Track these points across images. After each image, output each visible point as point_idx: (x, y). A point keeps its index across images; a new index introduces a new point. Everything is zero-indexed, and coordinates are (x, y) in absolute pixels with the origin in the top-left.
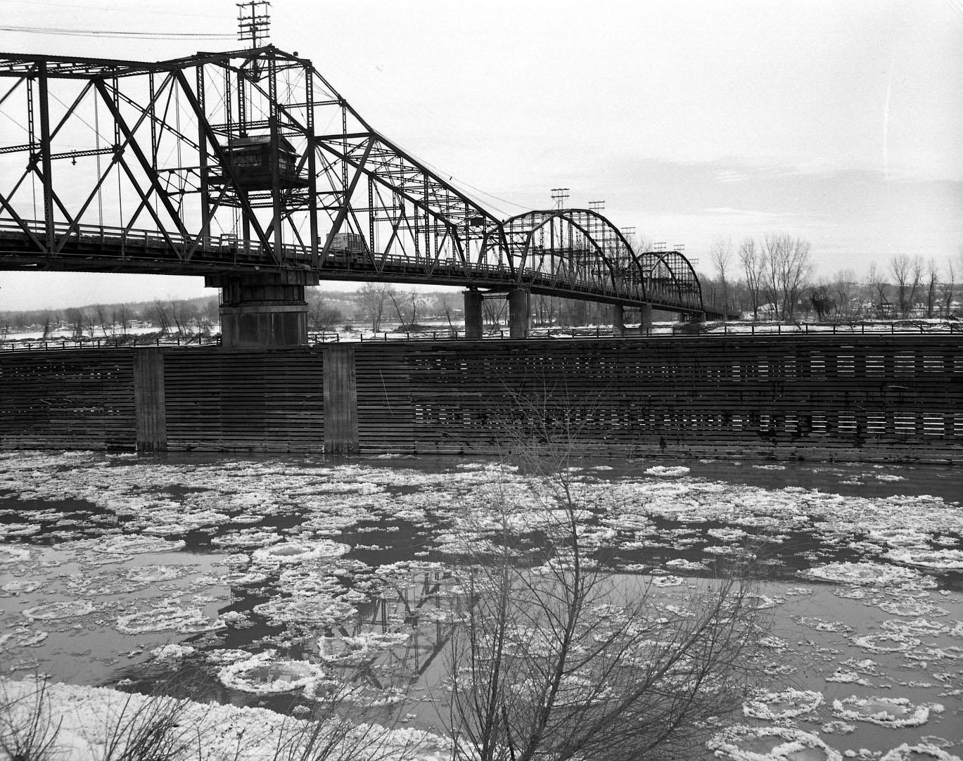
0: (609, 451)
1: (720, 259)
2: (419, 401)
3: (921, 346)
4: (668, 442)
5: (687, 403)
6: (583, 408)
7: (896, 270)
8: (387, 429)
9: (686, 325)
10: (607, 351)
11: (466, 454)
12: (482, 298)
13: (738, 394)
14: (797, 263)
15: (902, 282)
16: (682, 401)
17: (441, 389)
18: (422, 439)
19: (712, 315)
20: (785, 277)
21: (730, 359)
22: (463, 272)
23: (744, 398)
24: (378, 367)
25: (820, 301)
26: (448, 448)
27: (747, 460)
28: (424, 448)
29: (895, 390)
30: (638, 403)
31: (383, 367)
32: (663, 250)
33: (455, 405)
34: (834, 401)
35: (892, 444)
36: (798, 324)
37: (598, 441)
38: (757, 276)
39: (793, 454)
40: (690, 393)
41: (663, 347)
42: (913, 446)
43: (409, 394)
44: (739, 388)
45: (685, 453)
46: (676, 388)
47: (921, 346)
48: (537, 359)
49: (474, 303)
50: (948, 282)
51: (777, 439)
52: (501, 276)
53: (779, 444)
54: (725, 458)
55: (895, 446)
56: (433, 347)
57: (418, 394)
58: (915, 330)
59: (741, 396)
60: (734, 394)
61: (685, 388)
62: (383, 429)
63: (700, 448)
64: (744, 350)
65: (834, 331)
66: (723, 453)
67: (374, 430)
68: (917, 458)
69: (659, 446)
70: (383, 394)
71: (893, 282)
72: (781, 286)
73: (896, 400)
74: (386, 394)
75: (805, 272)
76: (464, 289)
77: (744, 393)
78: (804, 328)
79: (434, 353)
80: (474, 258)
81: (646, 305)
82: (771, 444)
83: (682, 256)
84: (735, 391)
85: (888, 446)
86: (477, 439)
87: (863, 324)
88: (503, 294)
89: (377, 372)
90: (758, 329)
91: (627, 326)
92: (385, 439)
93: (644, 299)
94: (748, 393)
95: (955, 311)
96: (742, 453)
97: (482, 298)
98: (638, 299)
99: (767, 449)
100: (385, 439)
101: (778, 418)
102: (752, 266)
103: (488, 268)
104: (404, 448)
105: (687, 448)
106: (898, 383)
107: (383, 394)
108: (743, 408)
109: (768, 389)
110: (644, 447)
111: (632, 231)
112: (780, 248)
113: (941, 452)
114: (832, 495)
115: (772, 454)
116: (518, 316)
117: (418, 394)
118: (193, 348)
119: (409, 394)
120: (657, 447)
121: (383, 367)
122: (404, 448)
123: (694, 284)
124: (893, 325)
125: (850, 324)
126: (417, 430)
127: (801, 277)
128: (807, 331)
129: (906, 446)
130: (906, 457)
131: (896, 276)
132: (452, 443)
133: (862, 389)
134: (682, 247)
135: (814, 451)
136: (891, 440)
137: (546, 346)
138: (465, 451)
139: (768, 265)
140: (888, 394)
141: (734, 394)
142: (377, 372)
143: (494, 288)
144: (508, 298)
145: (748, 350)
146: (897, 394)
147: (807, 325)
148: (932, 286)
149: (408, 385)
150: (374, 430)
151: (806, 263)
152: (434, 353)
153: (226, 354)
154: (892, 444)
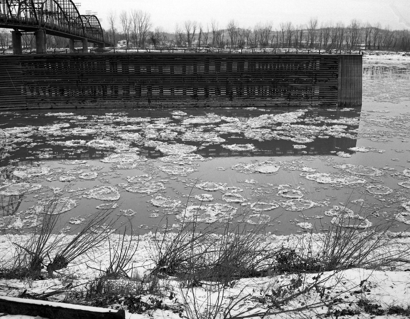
0: (125, 105)
1: (111, 19)
2: (27, 84)
3: (245, 58)
4: (152, 101)
5: (160, 83)
6: (112, 86)
7: (186, 27)
8: (11, 98)
9: (97, 49)
10: (123, 59)
11: (54, 109)
12: (21, 35)
13: (182, 79)
14: (145, 22)
15: (188, 32)
16: (158, 82)
17: (40, 78)
18: (30, 102)
19: (108, 45)
20: (140, 28)
21: (186, 64)
22: (18, 22)
23: (185, 81)
24: (6, 68)
25: (155, 39)
26: (44, 106)
27: (242, 106)
28: (32, 106)
29: (246, 77)
30: (138, 83)
31: (8, 68)
32: (90, 14)
33: (47, 85)
34: (104, 82)
35: (244, 99)
36: (147, 49)
37: (119, 101)
38: (128, 28)
39: (205, 104)
40: (162, 79)
41: (91, 57)
42: (252, 100)
43: (23, 80)
44: (183, 77)
45: (159, 105)
46: (46, 78)
47: (245, 58)
48: (93, 63)
49: (17, 36)
50: (207, 32)
51: (199, 98)
52: (33, 24)
53: (200, 100)
54: (177, 107)
55: (245, 100)
56: (34, 57)
57: (28, 80)
58: (194, 52)
59: (184, 80)
60: (181, 79)
61: (159, 77)
62: (9, 98)
63: (166, 103)
64: (136, 59)
65: (161, 52)
66: (175, 105)
67: (4, 99)
68: (253, 105)
69: (147, 102)
70: (10, 81)
71: (185, 32)
72: (139, 32)
73: (246, 81)
74: (11, 81)
75: (149, 27)
76: (12, 30)
77: (185, 79)
78: (149, 50)
79: (35, 60)
80: (14, 12)
81: (82, 39)
82: (196, 100)
83: (96, 17)
84: (182, 78)
85: (243, 100)
86: (59, 101)
87: (173, 49)
88: (32, 33)
89: (5, 70)
90: (139, 51)
91: (76, 48)
92: (10, 103)
93: (84, 37)
94: (187, 79)
95: (209, 44)
96: (184, 105)
97: (21, 35)
98: (82, 36)
99: (194, 103)
100: (10, 103)
101: (127, 89)
102: (125, 23)
103: (21, 19)
104: (21, 107)
105: (160, 103)
106: (247, 74)
107: (10, 81)
108: (185, 85)
109: (195, 77)
110: (141, 103)
111: (79, 4)
112: (137, 16)
113: (262, 101)
114: (158, 119)
115: (196, 104)
116: (39, 42)
117: (28, 80)
118: (141, 53)
119: (23, 80)
120: (146, 103)
121: (8, 68)
122: (21, 107)
123: (99, 31)
124: (185, 50)
125: (168, 50)
126: (28, 98)
127: (147, 28)
128: (150, 52)
129: (249, 100)
130: (249, 104)
131: (186, 29)
132: (46, 104)
133: (233, 76)
134: (96, 13)
135: (213, 103)
136: (244, 98)
137: (55, 58)
138: (54, 107)
139: (133, 23)
140: (243, 79)
141: (181, 79)
142: (5, 70)
143: (27, 30)
144: (35, 34)
145: (186, 59)
146: (247, 79)
147: (150, 49)
148: (200, 34)
149: (22, 76)
150: (4, 99)
151: (149, 23)
152: (35, 60)
153: (218, 58)
154: (244, 99)
